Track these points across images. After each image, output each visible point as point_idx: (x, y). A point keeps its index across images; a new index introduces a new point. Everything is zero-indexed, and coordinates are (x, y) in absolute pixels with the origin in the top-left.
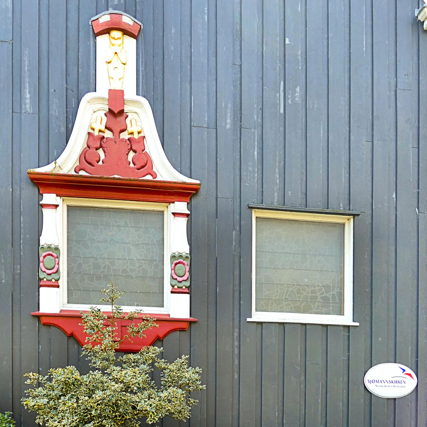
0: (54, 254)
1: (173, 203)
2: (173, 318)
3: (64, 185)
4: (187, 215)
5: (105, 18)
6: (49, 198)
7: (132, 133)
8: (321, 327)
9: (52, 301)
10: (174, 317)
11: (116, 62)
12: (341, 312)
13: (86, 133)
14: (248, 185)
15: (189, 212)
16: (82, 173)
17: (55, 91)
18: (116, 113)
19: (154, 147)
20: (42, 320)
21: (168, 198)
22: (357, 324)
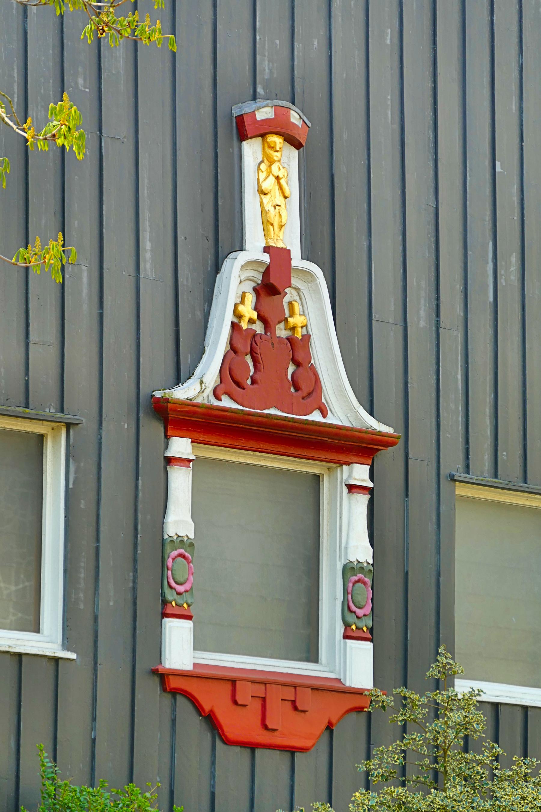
0: (187, 554)
1: (348, 464)
2: (169, 669)
4: (370, 491)
5: (265, 113)
6: (181, 446)
7: (293, 329)
8: (8, 656)
9: (180, 647)
10: (353, 686)
11: (271, 190)
13: (229, 325)
14: (449, 436)
15: (370, 485)
16: (226, 403)
17: (185, 238)
18: (269, 287)
20: (169, 682)
21: (342, 458)
22: (73, 656)
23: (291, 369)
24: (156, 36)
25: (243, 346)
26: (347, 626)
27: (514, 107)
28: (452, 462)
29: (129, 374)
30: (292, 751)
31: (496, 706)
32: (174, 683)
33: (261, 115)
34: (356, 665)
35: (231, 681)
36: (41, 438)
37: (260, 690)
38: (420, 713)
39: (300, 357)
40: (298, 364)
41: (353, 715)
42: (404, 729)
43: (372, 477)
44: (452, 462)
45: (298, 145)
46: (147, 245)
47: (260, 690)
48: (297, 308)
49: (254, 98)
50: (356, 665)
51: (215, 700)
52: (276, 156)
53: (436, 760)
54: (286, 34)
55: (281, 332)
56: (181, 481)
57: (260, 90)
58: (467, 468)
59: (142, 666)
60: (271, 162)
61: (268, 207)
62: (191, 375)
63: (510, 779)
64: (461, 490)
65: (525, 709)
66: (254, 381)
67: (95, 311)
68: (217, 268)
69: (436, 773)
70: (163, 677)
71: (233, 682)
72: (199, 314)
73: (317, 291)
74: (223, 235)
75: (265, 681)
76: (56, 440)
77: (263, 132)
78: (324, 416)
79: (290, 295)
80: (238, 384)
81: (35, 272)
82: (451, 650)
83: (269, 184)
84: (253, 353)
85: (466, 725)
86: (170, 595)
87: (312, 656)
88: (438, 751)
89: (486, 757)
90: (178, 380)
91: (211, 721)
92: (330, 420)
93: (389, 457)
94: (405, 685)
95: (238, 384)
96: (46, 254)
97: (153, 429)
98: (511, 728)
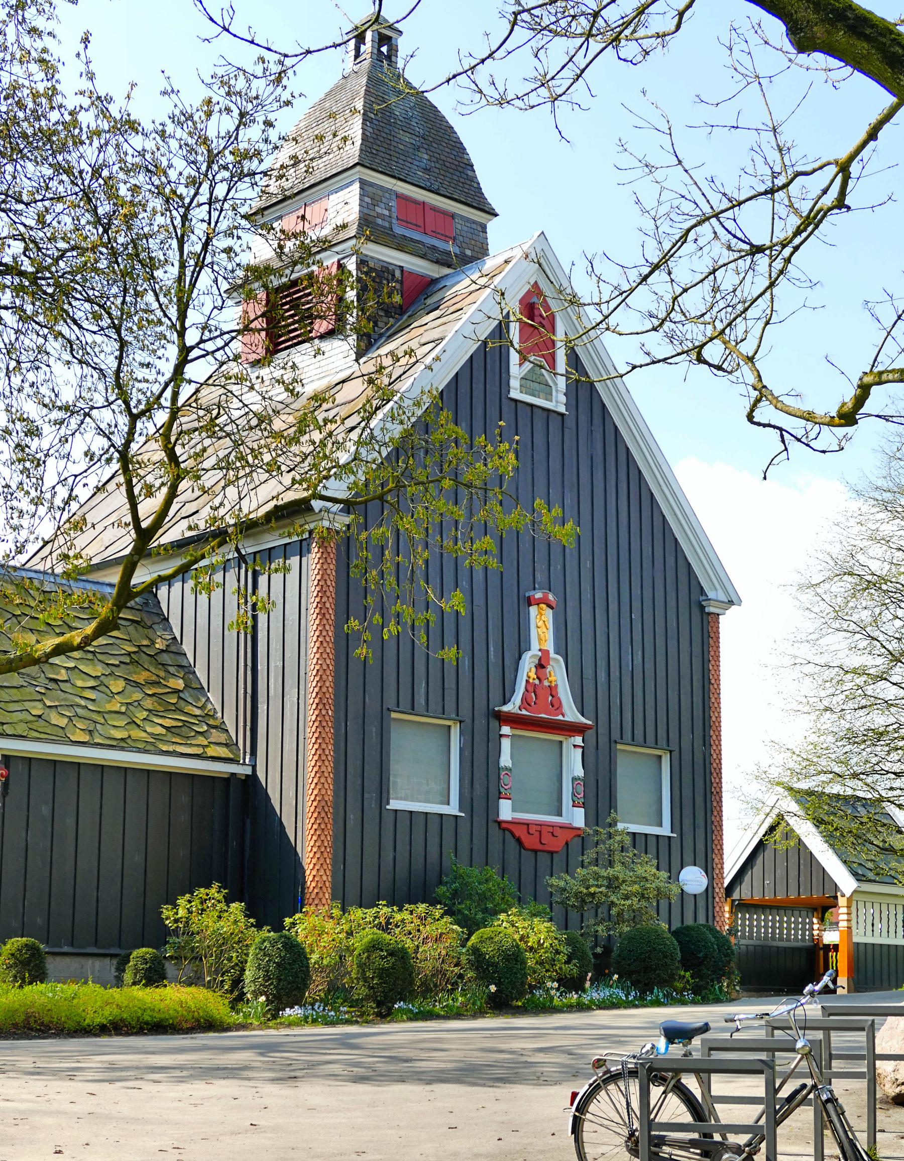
3: (515, 721)
4: (583, 747)
5: (539, 595)
6: (506, 730)
9: (506, 811)
11: (542, 626)
12: (660, 825)
16: (524, 712)
18: (541, 666)
19: (565, 694)
23: (550, 698)
24: (494, 565)
25: (531, 689)
26: (574, 802)
27: (639, 592)
28: (616, 735)
29: (485, 702)
30: (552, 853)
31: (634, 834)
32: (504, 825)
33: (537, 596)
34: (577, 818)
35: (527, 825)
36: (449, 727)
37: (539, 828)
38: (604, 837)
39: (553, 693)
40: (553, 697)
41: (577, 838)
42: (597, 843)
43: (583, 742)
44: (616, 735)
45: (552, 608)
46: (492, 649)
47: (539, 828)
48: (553, 674)
49: (534, 589)
50: (577, 818)
51: (520, 832)
52: (543, 612)
53: (610, 856)
54: (547, 563)
55: (546, 683)
56: (506, 744)
57: (537, 586)
58: (622, 738)
59: (491, 818)
60: (541, 615)
61: (541, 633)
62: (510, 701)
63: (640, 864)
64: (619, 747)
65: (646, 835)
66: (535, 703)
67: (471, 675)
68: (520, 658)
69: (610, 861)
70: (499, 823)
71: (528, 825)
72: (513, 676)
73: (561, 667)
74: (522, 646)
75: (540, 825)
76: (455, 727)
77: (538, 603)
78: (564, 716)
79: (549, 668)
80: (529, 705)
81: (446, 660)
82: (616, 811)
83: (540, 624)
84: (535, 692)
85: (622, 842)
86: (502, 790)
87: (560, 814)
88: (611, 852)
89: (631, 855)
90: (505, 703)
91: (519, 841)
92: (566, 719)
93: (590, 733)
94: (597, 825)
95: (529, 705)
96: (450, 653)
97: (494, 723)
98: (641, 843)
